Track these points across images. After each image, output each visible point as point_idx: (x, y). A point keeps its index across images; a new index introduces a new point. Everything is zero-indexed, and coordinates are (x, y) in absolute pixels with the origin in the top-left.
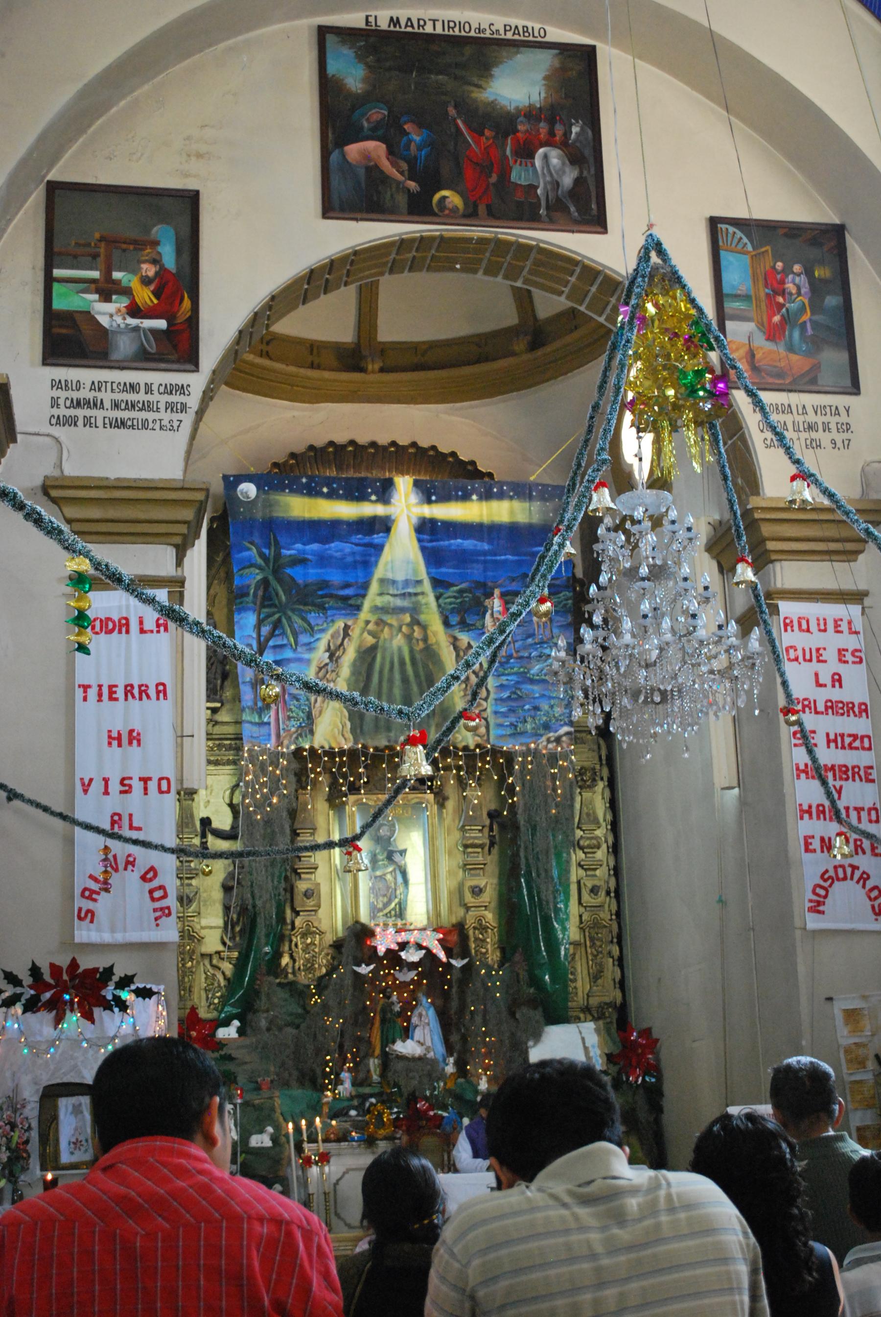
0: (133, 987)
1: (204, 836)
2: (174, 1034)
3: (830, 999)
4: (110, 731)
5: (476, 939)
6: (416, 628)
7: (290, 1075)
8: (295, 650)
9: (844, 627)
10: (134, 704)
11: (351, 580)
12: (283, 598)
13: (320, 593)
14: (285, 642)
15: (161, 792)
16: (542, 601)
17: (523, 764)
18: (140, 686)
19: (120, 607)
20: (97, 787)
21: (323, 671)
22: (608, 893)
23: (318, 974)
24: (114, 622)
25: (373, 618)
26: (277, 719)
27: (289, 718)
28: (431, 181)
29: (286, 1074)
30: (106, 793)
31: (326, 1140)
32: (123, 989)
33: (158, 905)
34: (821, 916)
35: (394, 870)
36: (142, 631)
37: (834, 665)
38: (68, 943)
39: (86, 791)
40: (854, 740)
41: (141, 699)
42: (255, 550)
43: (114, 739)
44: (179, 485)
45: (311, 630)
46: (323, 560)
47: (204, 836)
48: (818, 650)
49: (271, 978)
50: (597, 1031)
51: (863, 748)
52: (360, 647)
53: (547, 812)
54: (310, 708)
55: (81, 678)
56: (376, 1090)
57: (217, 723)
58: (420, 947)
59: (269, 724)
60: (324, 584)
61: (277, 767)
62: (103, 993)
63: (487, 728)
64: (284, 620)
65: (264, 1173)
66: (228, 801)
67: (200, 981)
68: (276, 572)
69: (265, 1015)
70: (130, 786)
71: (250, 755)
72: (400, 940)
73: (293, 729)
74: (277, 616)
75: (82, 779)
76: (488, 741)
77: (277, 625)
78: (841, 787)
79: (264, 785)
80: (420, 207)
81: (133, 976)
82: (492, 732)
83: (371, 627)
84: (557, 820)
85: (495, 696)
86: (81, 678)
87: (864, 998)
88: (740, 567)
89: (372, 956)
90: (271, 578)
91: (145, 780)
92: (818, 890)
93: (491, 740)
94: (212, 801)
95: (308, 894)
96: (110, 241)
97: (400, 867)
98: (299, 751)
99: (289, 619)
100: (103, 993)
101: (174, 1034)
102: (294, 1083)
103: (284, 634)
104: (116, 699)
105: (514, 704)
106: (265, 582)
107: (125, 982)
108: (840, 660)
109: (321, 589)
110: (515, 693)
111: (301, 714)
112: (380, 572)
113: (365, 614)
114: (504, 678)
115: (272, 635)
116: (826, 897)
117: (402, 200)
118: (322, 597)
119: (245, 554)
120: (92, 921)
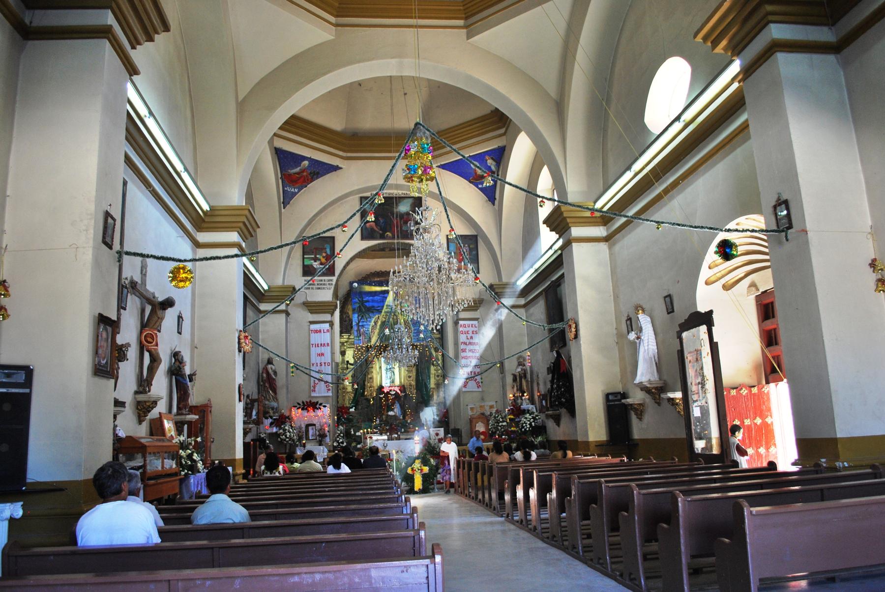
2: (28, 481)
28: (385, 231)
37: (471, 334)
38: (310, 396)
43: (319, 355)
45: (370, 317)
46: (373, 301)
80: (382, 237)
96: (316, 249)
101: (28, 481)
107: (321, 404)
117: (378, 236)
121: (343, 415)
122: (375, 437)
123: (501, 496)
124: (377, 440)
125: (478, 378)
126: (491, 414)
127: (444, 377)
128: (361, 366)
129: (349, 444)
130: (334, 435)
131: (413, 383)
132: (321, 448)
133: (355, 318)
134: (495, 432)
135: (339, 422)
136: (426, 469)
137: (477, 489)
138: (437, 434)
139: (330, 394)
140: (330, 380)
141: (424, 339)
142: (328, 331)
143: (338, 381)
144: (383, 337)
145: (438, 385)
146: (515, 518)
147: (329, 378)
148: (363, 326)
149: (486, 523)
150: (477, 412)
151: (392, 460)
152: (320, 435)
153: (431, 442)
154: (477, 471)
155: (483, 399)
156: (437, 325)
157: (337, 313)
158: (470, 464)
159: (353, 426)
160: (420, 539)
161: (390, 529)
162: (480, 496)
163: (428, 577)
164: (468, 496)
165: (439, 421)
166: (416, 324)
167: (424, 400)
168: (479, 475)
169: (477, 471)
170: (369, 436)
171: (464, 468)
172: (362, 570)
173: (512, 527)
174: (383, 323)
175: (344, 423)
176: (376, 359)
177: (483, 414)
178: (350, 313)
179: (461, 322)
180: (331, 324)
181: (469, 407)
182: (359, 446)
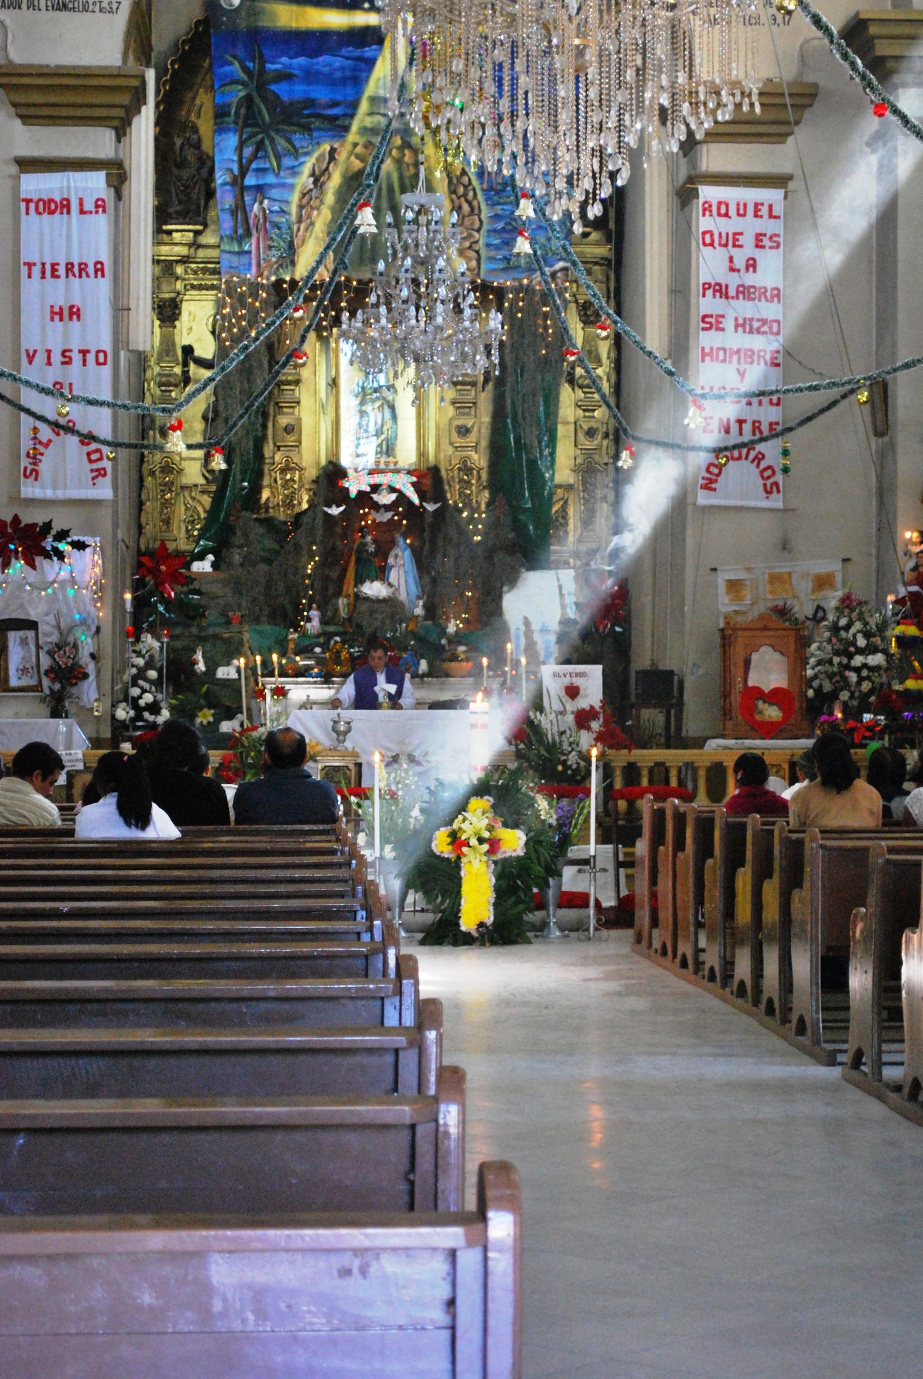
0: (69, 540)
1: (185, 364)
3: (714, 570)
4: (52, 307)
5: (461, 481)
6: (407, 152)
7: (261, 610)
8: (277, 175)
9: (764, 211)
10: (75, 282)
11: (339, 97)
12: (267, 118)
13: (306, 112)
14: (267, 165)
15: (98, 363)
16: (296, 310)
17: (513, 303)
18: (80, 264)
19: (61, 189)
20: (40, 358)
21: (307, 197)
22: (606, 435)
23: (297, 510)
24: (56, 203)
25: (361, 141)
26: (258, 248)
27: (270, 247)
29: (257, 609)
30: (49, 363)
31: (281, 675)
32: (60, 541)
33: (95, 466)
34: (712, 493)
35: (382, 405)
36: (82, 212)
38: (15, 498)
39: (30, 362)
40: (758, 328)
41: (80, 277)
42: (237, 64)
43: (57, 314)
44: (115, 73)
45: (295, 153)
46: (311, 76)
47: (185, 364)
48: (735, 234)
49: (246, 514)
50: (576, 578)
51: (772, 333)
52: (346, 170)
53: (536, 352)
54: (292, 237)
55: (30, 253)
56: (341, 629)
57: (199, 246)
58: (392, 489)
59: (249, 252)
60: (310, 103)
61: (256, 299)
62: (43, 544)
63: (479, 261)
64: (267, 142)
65: (228, 703)
66: (210, 328)
67: (181, 512)
68: (261, 88)
69: (239, 551)
70: (70, 358)
71: (228, 287)
72: (372, 482)
73: (274, 259)
74: (260, 137)
75: (27, 351)
76: (478, 275)
77: (260, 146)
78: (745, 371)
79: (242, 317)
81: (69, 531)
82: (483, 266)
83: (359, 149)
84: (546, 360)
85: (489, 227)
86: (30, 253)
87: (748, 570)
88: (520, 239)
89: (342, 496)
90: (254, 94)
91: (84, 352)
92: (712, 469)
93: (482, 275)
94: (194, 328)
95: (289, 429)
97: (388, 402)
98: (280, 281)
99: (272, 141)
100: (43, 544)
102: (264, 619)
103: (266, 156)
104: (58, 277)
105: (508, 236)
106: (248, 99)
107: (62, 535)
108: (757, 246)
109: (306, 108)
110: (510, 224)
111: (282, 244)
112: (370, 89)
113: (353, 136)
114: (499, 207)
115: (255, 157)
116: (718, 475)
118: (309, 116)
119: (227, 69)
120: (36, 479)
121: (159, 589)
122: (299, 691)
123: (833, 975)
124: (304, 706)
125: (771, 450)
126: (819, 614)
127: (618, 437)
128: (246, 369)
129: (184, 712)
130: (118, 672)
131: (480, 460)
132: (61, 725)
133: (226, 151)
134: (833, 696)
135: (140, 620)
136: (514, 842)
137: (731, 936)
138: (573, 692)
139: (104, 491)
140: (105, 430)
141: (536, 262)
142: (100, 205)
143: (143, 435)
144: (344, 240)
145: (587, 470)
146: (889, 1073)
147: (101, 423)
148: (260, 189)
149: (759, 1088)
150: (755, 604)
151: (363, 794)
152: (55, 672)
153: (546, 722)
154: (734, 861)
155: (785, 546)
156: (590, 197)
157: (145, 125)
158: (705, 825)
159: (202, 639)
160: (438, 1136)
161: (287, 1090)
162: (743, 968)
163: (451, 1303)
164: (692, 965)
165: (586, 636)
166: (503, 191)
167: (524, 539)
168: (744, 879)
169: (734, 861)
170: (271, 683)
171: (680, 845)
172: (169, 1256)
173: (874, 1108)
174: (353, 181)
175: (165, 623)
176: (312, 344)
177: (782, 612)
178: (205, 126)
179: (708, 193)
180: (118, 174)
181: (722, 578)
182: (226, 727)
